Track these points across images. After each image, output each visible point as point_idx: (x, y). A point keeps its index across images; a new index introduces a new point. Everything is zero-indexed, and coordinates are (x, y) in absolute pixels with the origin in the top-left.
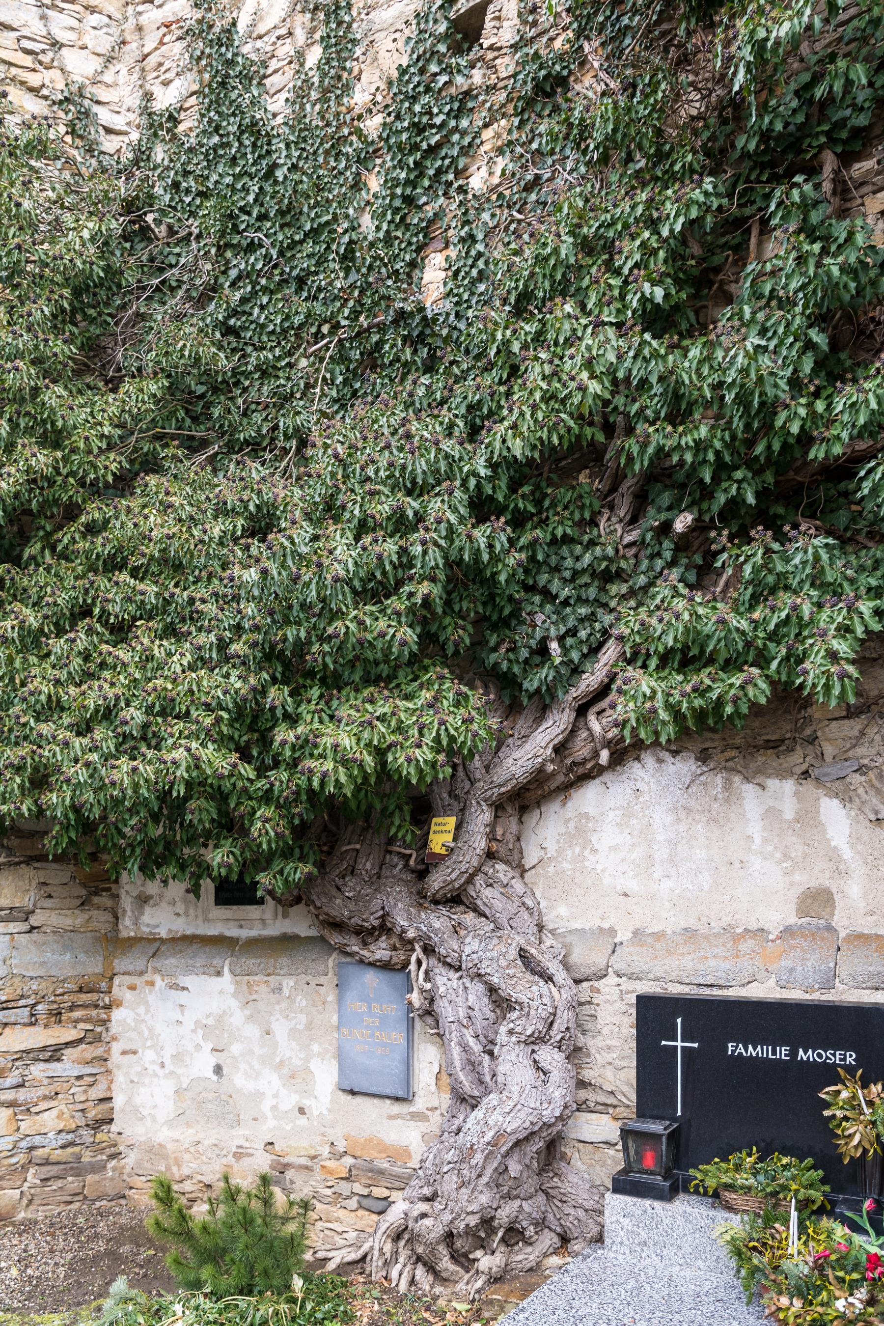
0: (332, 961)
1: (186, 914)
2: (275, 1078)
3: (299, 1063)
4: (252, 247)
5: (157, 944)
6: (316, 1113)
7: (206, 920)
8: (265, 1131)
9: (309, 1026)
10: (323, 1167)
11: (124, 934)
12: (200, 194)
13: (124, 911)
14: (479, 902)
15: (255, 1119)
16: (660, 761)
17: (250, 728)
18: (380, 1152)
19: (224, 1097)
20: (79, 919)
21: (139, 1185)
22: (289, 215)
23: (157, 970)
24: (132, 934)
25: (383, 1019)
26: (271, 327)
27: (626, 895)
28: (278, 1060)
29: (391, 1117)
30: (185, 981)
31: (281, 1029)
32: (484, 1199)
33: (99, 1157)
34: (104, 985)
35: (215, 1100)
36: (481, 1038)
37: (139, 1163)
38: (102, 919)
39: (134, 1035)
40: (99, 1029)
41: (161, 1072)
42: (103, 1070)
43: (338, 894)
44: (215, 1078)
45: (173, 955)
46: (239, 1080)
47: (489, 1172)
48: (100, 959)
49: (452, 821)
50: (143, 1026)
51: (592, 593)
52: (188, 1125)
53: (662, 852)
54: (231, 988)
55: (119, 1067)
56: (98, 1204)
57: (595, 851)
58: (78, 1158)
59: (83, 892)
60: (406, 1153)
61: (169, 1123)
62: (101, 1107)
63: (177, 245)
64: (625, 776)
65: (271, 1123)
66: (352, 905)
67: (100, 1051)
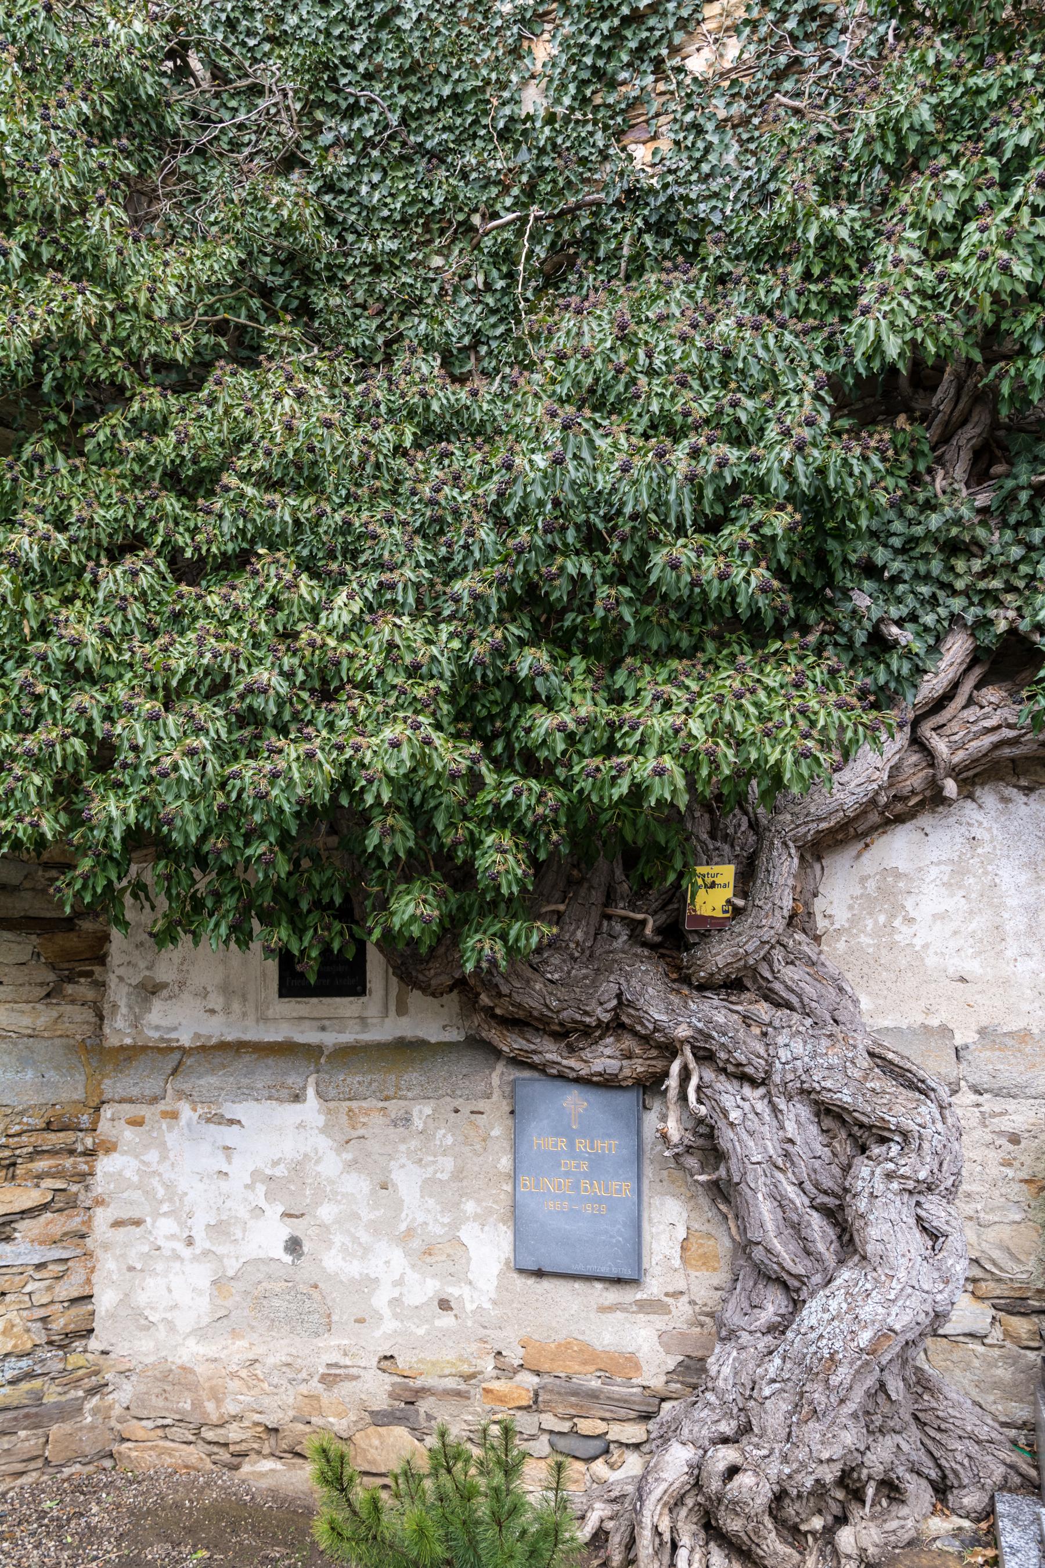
0: (499, 1075)
1: (227, 1011)
2: (397, 1257)
3: (439, 1230)
4: (353, 111)
5: (176, 1056)
6: (470, 1307)
7: (263, 1019)
8: (382, 1335)
9: (458, 1175)
10: (487, 1391)
11: (113, 1040)
12: (270, 39)
13: (115, 1006)
14: (777, 986)
15: (360, 1321)
16: (1005, 800)
17: (484, 705)
18: (585, 1363)
19: (303, 1288)
20: (43, 1017)
21: (140, 1434)
22: (412, 75)
23: (181, 1095)
24: (128, 1041)
25: (596, 1162)
26: (386, 213)
27: (963, 980)
28: (403, 1227)
29: (603, 1309)
30: (231, 1110)
31: (407, 1180)
32: (848, 1438)
33: (73, 1394)
34: (85, 1119)
35: (291, 1293)
36: (808, 1186)
37: (141, 1400)
38: (78, 1018)
39: (137, 1195)
40: (74, 1188)
41: (186, 1252)
42: (79, 1252)
43: (535, 976)
44: (288, 1259)
45: (212, 1071)
46: (332, 1261)
47: (858, 1396)
48: (80, 1078)
49: (726, 873)
50: (155, 1182)
51: (936, 567)
52: (235, 1334)
53: (1015, 923)
54: (321, 1120)
55: (106, 1246)
56: (67, 1471)
57: (910, 921)
58: (38, 1397)
59: (51, 977)
60: (632, 1362)
61: (201, 1333)
62: (74, 1311)
63: (232, 96)
64: (952, 820)
65: (390, 1325)
66: (562, 993)
67: (75, 1223)
